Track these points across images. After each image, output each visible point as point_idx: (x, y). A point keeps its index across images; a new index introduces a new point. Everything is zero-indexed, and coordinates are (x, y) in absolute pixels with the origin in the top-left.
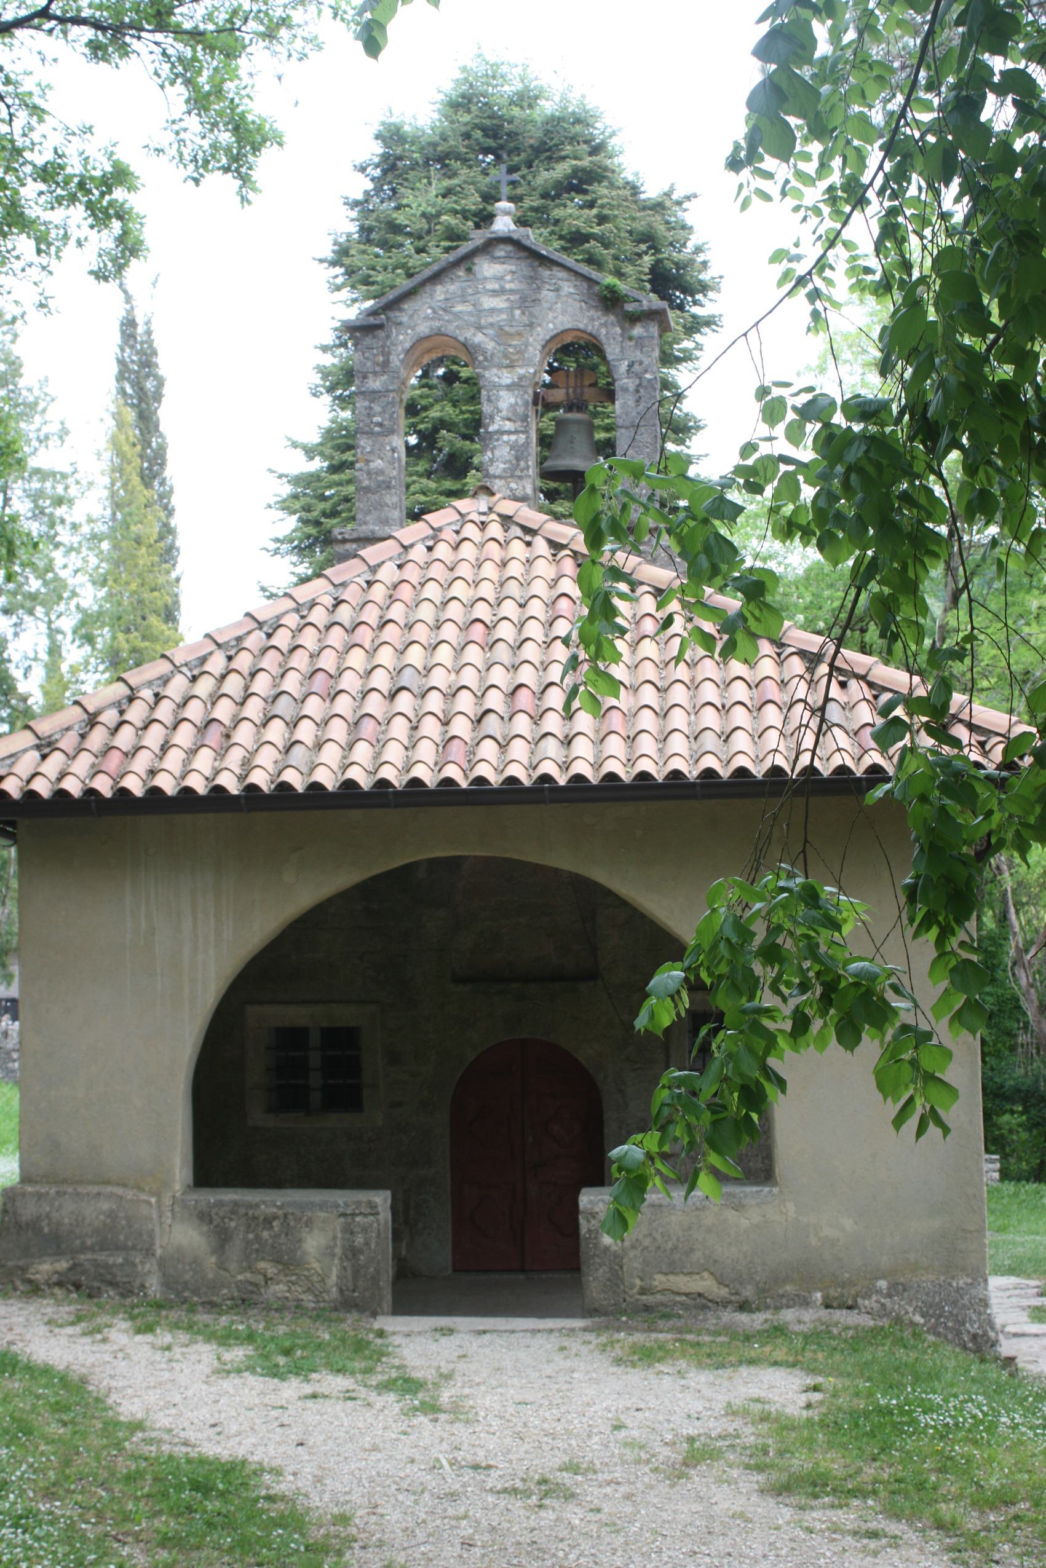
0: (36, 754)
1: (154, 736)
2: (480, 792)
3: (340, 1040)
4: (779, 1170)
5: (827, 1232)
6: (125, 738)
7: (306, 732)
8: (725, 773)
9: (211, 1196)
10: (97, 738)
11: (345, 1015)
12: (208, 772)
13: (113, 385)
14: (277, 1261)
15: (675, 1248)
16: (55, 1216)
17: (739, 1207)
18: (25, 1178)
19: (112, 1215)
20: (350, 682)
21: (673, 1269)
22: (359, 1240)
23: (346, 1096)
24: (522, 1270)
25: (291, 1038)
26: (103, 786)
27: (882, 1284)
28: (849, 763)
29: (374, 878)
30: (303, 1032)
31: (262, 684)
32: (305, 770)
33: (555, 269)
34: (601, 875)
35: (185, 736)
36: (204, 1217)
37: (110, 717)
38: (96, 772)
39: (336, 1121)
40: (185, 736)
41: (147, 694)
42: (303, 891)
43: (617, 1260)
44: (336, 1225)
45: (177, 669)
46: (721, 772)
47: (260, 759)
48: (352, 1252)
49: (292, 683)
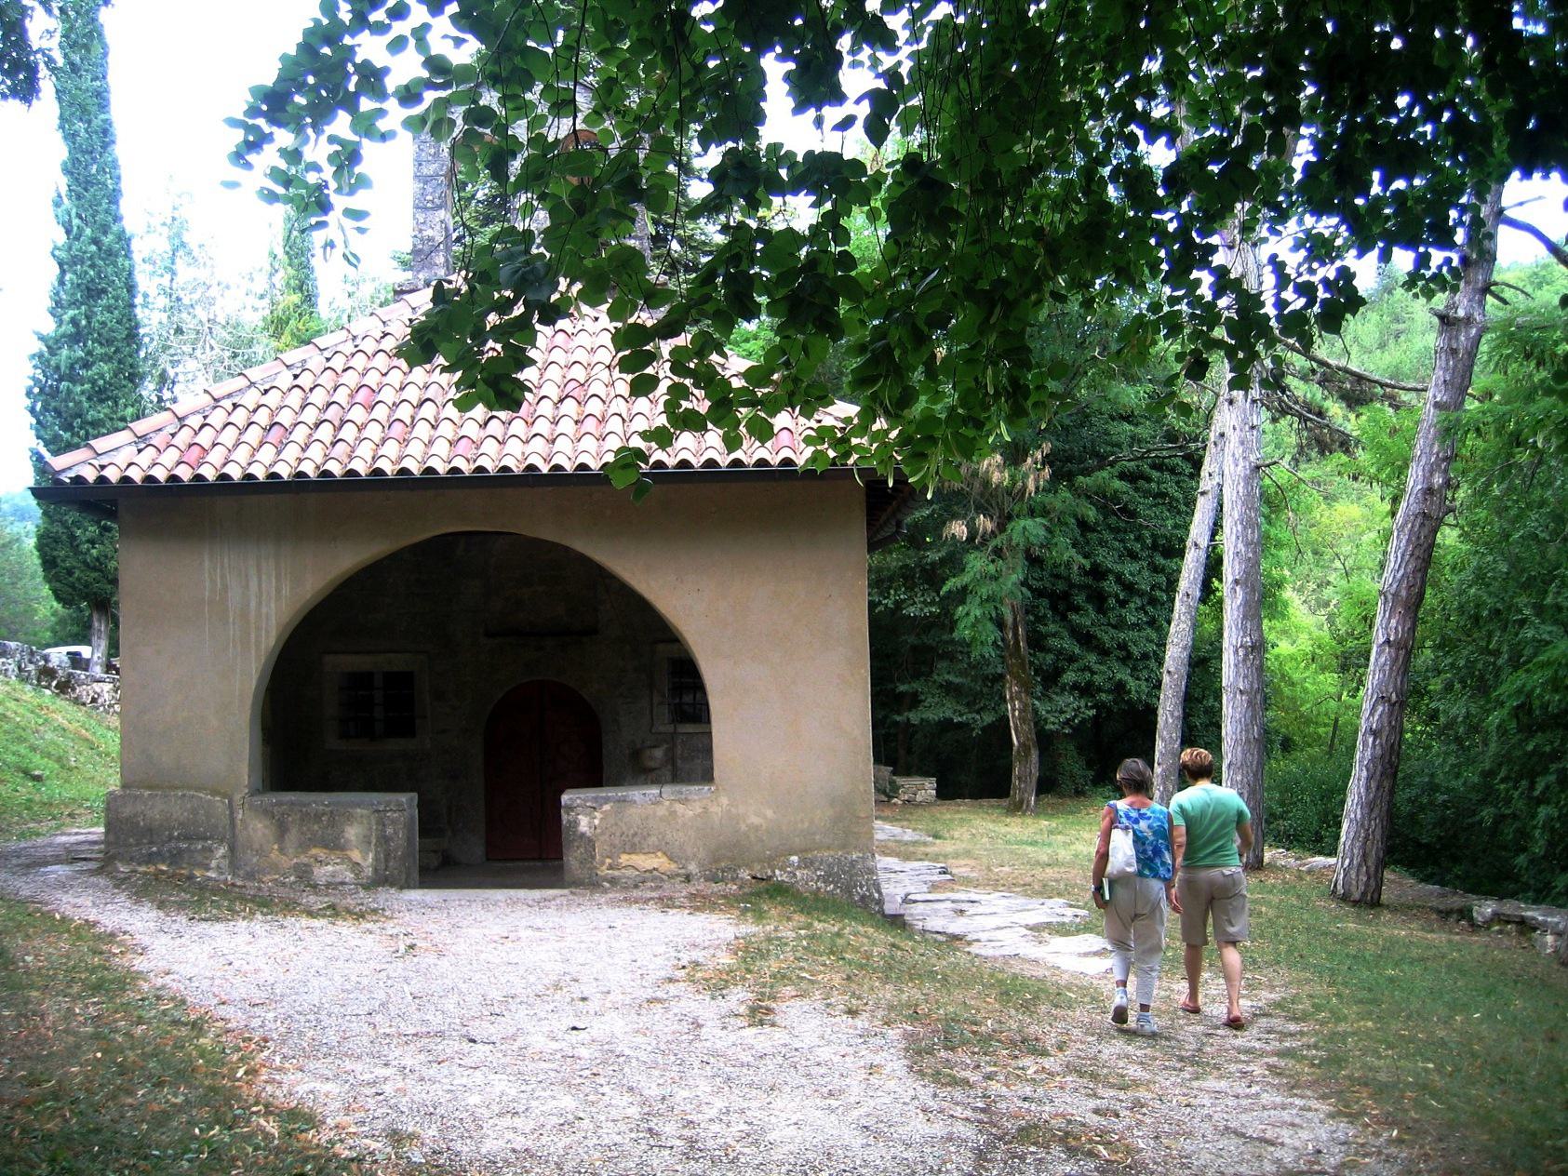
0: (134, 449)
1: (229, 436)
2: (505, 478)
3: (400, 683)
4: (716, 774)
5: (755, 820)
6: (205, 438)
7: (349, 432)
8: (545, 469)
9: (273, 798)
10: (184, 437)
11: (399, 662)
12: (319, 461)
13: (123, 185)
14: (326, 847)
15: (635, 834)
16: (149, 813)
17: (685, 801)
18: (124, 786)
19: (194, 811)
20: (388, 395)
21: (633, 849)
22: (389, 831)
23: (403, 725)
24: (540, 859)
25: (359, 681)
26: (185, 473)
27: (795, 858)
28: (768, 457)
29: (402, 551)
30: (370, 675)
31: (319, 397)
32: (369, 460)
33: (139, 215)
34: (580, 545)
35: (253, 435)
36: (267, 813)
37: (195, 421)
38: (327, 458)
39: (395, 745)
40: (253, 435)
41: (227, 404)
42: (346, 559)
43: (590, 842)
44: (368, 822)
45: (252, 384)
46: (694, 461)
47: (302, 456)
48: (384, 840)
49: (342, 396)
